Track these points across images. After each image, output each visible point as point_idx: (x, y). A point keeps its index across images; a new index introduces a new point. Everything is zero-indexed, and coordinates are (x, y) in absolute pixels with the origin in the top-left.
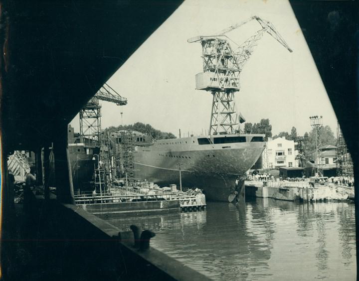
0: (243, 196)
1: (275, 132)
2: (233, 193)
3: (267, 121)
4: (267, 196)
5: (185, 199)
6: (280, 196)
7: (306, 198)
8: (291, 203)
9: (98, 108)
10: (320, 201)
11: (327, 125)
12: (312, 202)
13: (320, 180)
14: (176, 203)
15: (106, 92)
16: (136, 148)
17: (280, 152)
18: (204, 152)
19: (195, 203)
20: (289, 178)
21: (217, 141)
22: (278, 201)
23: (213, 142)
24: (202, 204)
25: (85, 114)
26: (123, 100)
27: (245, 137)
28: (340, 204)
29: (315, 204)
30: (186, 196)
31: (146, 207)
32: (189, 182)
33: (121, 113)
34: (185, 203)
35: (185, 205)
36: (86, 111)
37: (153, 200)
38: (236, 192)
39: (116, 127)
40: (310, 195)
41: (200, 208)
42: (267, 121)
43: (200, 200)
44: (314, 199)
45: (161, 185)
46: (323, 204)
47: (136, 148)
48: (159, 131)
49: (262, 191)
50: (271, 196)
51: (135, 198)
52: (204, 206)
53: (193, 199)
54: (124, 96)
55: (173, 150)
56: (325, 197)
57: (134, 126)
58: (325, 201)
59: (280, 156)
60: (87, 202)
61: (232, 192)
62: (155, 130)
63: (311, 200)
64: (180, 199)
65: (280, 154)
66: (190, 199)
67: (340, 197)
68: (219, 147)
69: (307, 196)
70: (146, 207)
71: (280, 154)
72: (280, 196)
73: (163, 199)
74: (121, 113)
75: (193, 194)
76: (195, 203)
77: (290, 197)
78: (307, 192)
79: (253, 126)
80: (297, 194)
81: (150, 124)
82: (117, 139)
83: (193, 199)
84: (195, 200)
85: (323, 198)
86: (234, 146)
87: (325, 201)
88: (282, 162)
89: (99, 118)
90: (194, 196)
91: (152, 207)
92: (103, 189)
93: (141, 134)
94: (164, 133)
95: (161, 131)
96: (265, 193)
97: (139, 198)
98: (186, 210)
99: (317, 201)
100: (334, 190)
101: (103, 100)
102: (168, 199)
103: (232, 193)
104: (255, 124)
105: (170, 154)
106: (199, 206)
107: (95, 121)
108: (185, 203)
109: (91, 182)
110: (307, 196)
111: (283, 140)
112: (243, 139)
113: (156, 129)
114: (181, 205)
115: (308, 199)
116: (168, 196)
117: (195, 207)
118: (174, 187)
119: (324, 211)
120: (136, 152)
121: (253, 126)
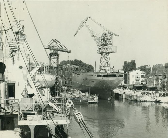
0: (114, 98)
1: (137, 66)
2: (110, 97)
3: (134, 61)
4: (125, 98)
5: (90, 99)
6: (129, 99)
7: (138, 100)
8: (133, 102)
9: (58, 55)
10: (144, 101)
11: (161, 63)
12: (141, 101)
13: (146, 93)
14: (86, 101)
15: (62, 48)
16: (73, 74)
17: (138, 76)
18: (99, 80)
19: (94, 101)
20: (136, 90)
21: (105, 76)
22: (128, 100)
23: (103, 76)
24: (97, 101)
25: (52, 58)
26: (69, 51)
27: (116, 75)
28: (152, 103)
29: (142, 103)
30: (90, 98)
31: (75, 102)
32: (92, 92)
33: (68, 57)
34: (90, 100)
35: (90, 101)
36: (53, 56)
37: (77, 99)
38: (111, 96)
39: (66, 61)
40: (140, 99)
41: (96, 103)
42: (134, 61)
43: (96, 100)
44: (142, 100)
45: (83, 91)
46: (145, 102)
47: (73, 74)
48: (85, 63)
49: (123, 96)
50: (126, 98)
51: (70, 98)
52: (97, 102)
53: (93, 99)
54: (69, 49)
55: (88, 78)
56: (146, 100)
57: (74, 61)
58: (146, 101)
59: (137, 78)
60: (120, 134)
61: (110, 96)
62: (83, 63)
63: (140, 101)
64: (88, 99)
65: (138, 77)
66: (92, 99)
67: (152, 100)
68: (105, 78)
69: (139, 99)
70: (75, 102)
71: (138, 77)
72: (129, 99)
73: (81, 99)
74: (68, 57)
75: (93, 97)
76: (94, 101)
77: (133, 99)
78: (139, 98)
79: (128, 63)
80: (135, 98)
81: (81, 60)
82: (66, 68)
83: (93, 99)
84: (94, 100)
85: (145, 100)
86: (110, 79)
87: (146, 101)
88: (138, 81)
89: (58, 60)
90: (93, 98)
91: (77, 102)
92: (58, 94)
93: (76, 66)
94: (87, 65)
95: (86, 64)
96: (124, 97)
97: (72, 98)
98: (90, 103)
99: (143, 101)
100: (150, 97)
101: (60, 51)
102: (83, 99)
103: (110, 97)
104: (129, 62)
105: (86, 79)
106: (95, 102)
107: (56, 61)
108: (90, 100)
109: (54, 91)
110: (139, 99)
111: (139, 71)
112: (115, 76)
113: (83, 62)
114: (88, 101)
115: (139, 101)
116: (83, 98)
117: (94, 102)
118: (87, 93)
119: (17, 111)
120: (73, 76)
121: (128, 63)
